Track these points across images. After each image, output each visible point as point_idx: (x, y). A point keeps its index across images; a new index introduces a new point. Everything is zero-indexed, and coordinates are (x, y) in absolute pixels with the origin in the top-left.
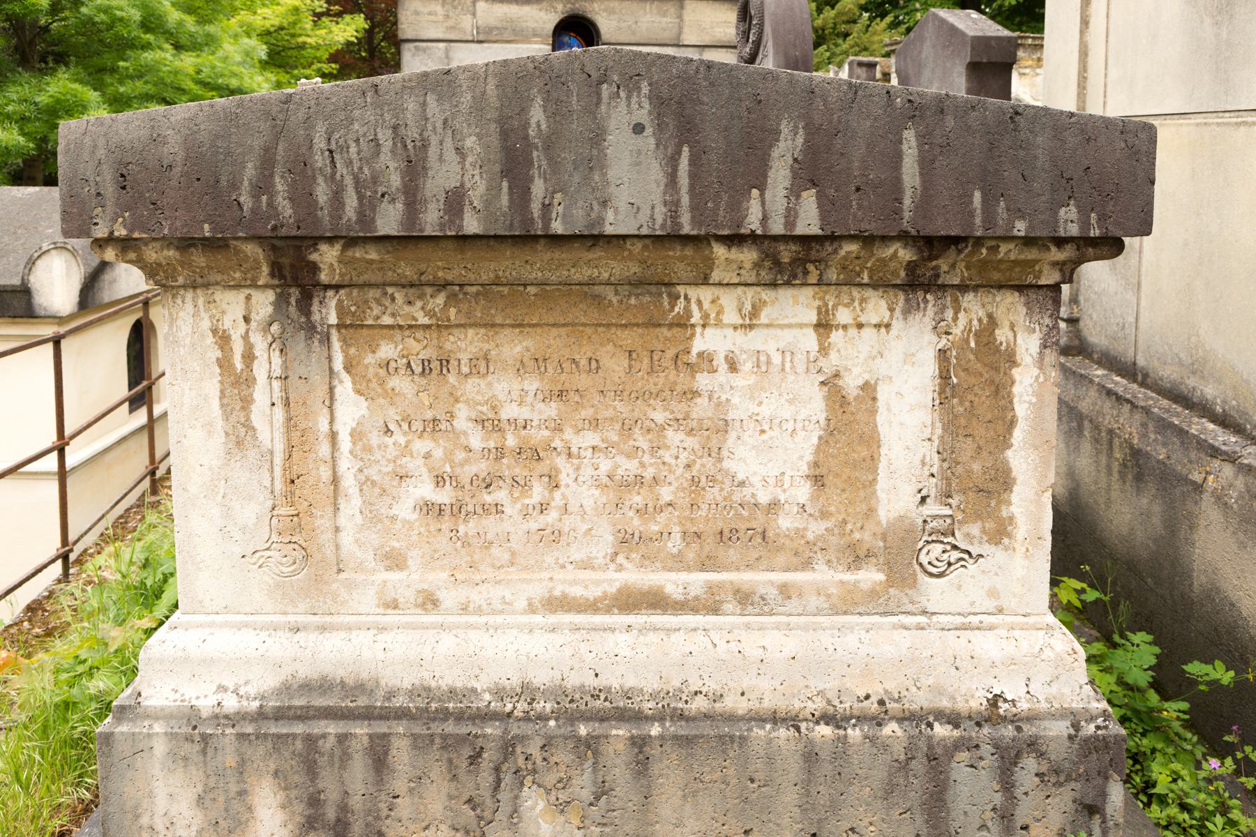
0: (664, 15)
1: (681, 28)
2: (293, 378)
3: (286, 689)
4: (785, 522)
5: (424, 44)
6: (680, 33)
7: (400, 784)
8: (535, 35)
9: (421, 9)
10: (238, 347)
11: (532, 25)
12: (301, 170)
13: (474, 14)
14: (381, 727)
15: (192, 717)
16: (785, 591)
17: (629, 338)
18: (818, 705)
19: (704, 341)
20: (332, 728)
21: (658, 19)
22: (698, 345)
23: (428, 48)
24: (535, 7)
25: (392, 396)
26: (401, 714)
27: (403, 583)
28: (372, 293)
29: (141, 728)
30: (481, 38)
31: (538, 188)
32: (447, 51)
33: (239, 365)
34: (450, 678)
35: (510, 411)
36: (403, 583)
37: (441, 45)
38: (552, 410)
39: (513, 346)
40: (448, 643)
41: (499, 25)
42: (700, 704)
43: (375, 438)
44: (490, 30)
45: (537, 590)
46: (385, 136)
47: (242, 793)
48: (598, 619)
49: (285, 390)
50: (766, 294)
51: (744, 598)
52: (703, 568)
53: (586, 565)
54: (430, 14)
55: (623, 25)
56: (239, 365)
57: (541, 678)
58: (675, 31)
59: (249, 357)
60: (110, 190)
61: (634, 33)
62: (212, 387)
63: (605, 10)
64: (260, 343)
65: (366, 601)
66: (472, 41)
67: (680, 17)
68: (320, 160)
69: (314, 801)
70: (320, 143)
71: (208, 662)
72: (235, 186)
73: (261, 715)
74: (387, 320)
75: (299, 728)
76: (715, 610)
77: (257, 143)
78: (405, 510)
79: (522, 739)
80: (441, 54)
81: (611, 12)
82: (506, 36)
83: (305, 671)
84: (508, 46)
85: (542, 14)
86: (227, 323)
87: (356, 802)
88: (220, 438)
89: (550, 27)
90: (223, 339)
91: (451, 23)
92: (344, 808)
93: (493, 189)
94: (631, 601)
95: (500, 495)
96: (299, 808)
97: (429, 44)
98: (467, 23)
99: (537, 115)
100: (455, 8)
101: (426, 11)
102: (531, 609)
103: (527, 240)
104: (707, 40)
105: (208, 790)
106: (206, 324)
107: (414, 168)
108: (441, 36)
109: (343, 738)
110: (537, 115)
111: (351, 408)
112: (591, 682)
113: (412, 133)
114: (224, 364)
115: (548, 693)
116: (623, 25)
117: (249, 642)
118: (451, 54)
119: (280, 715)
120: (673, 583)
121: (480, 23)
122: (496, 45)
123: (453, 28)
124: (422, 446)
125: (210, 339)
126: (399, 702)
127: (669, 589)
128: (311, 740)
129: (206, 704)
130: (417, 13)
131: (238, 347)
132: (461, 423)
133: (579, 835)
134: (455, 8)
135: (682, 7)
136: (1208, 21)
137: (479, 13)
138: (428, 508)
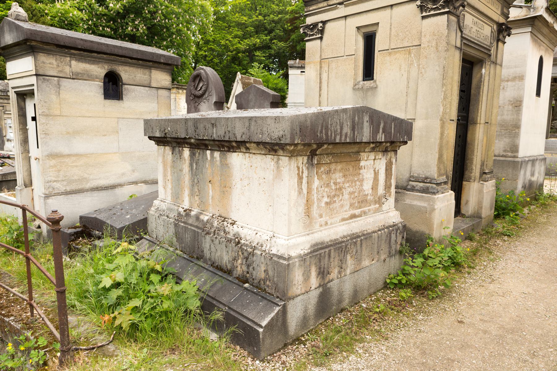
0: (145, 75)
1: (151, 80)
2: (309, 177)
3: (311, 247)
4: (369, 197)
5: (48, 78)
6: (150, 82)
7: (332, 260)
8: (97, 78)
9: (45, 61)
10: (301, 170)
11: (95, 73)
12: (327, 129)
13: (70, 66)
14: (329, 249)
15: (300, 256)
16: (369, 210)
17: (353, 163)
18: (377, 229)
19: (362, 163)
20: (323, 251)
21: (143, 76)
22: (361, 164)
23: (49, 79)
24: (97, 66)
25: (322, 179)
26: (331, 245)
27: (323, 220)
28: (322, 156)
29: (293, 261)
30: (74, 77)
31: (356, 133)
32: (58, 81)
33: (301, 174)
34: (334, 237)
35: (338, 180)
36: (323, 220)
37: (56, 79)
38: (343, 179)
39: (339, 166)
40: (332, 231)
41: (81, 72)
42: (365, 232)
43: (320, 189)
44: (78, 74)
45: (340, 218)
46: (338, 121)
47: (310, 270)
48: (348, 221)
49: (308, 179)
50: (369, 154)
51: (365, 213)
52: (360, 208)
53: (346, 211)
54: (50, 64)
55: (131, 77)
56: (301, 174)
57: (345, 234)
58: (149, 81)
59: (302, 172)
60: (298, 132)
61: (134, 81)
62: (296, 180)
63: (124, 70)
64: (304, 168)
65: (317, 226)
66: (70, 78)
67: (150, 76)
68: (329, 126)
69: (320, 268)
70: (330, 123)
71: (298, 245)
72: (317, 132)
73: (311, 252)
74: (324, 162)
75: (318, 253)
76: (361, 216)
77: (321, 122)
78: (323, 205)
79: (348, 245)
80: (56, 82)
81: (126, 71)
82: (85, 77)
83: (314, 242)
84: (85, 81)
85: (99, 69)
86: (299, 165)
87: (326, 266)
88: (297, 192)
89: (103, 75)
90: (298, 168)
91: (60, 69)
92: (324, 268)
93: (351, 133)
94: (353, 216)
95: (336, 199)
96: (318, 270)
97: (50, 78)
98: (67, 69)
99: (356, 118)
100: (62, 62)
101: (48, 62)
102: (340, 222)
103: (355, 143)
104: (159, 86)
105: (305, 271)
106: (296, 165)
107: (342, 129)
108: (56, 74)
109: (325, 252)
110: (356, 118)
111: (316, 183)
112: (352, 233)
113: (341, 121)
114: (298, 174)
115: (349, 236)
116: (131, 77)
117: (303, 239)
118: (60, 83)
119: (314, 251)
120: (357, 212)
121: (73, 70)
122: (80, 81)
123: (61, 71)
124: (326, 189)
125: (296, 169)
126: (330, 243)
127: (357, 214)
128: (320, 254)
129: (302, 252)
130: (44, 63)
131: (301, 170)
132: (332, 184)
133: (172, 370)
134: (62, 62)
135: (151, 72)
136: (360, 99)
137: (73, 66)
138: (327, 203)
